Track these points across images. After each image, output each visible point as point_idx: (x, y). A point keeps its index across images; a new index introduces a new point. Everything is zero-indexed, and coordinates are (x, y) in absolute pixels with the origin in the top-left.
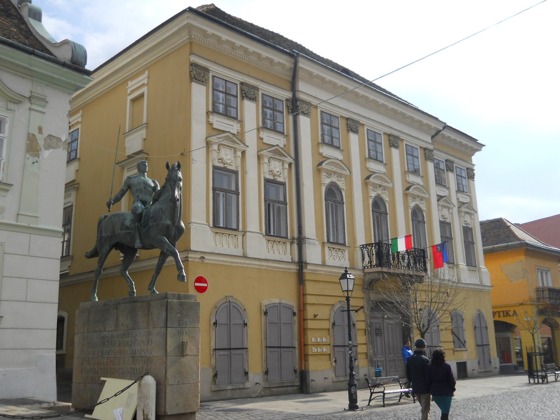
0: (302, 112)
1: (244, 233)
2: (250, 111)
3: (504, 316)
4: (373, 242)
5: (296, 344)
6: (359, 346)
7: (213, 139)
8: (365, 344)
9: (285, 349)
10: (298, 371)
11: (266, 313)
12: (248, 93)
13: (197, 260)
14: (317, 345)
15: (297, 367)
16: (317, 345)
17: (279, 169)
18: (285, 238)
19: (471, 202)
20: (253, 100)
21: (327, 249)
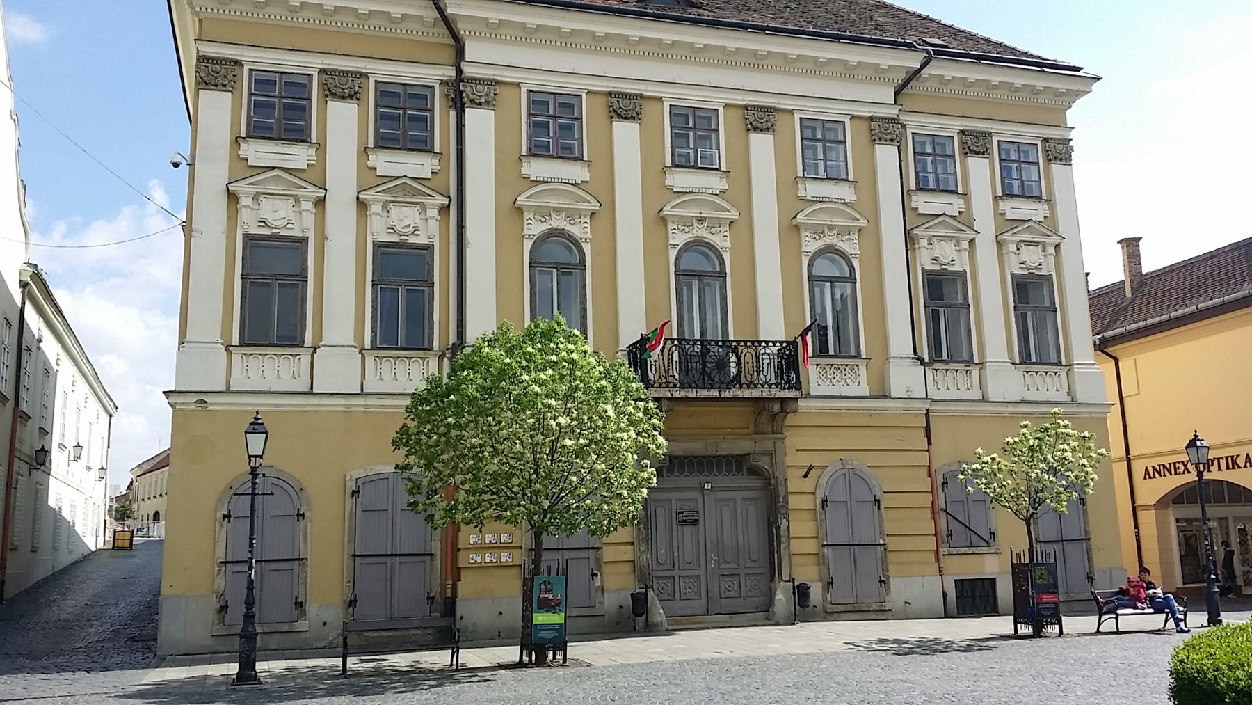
0: (472, 101)
1: (982, 364)
2: (343, 124)
3: (1228, 468)
4: (675, 336)
5: (437, 548)
6: (605, 548)
7: (1008, 236)
8: (633, 543)
9: (274, 566)
10: (438, 599)
11: (356, 493)
12: (975, 144)
13: (193, 407)
14: (481, 548)
15: (436, 592)
16: (481, 548)
17: (419, 224)
18: (854, 357)
19: (1051, 219)
20: (351, 97)
21: (370, 361)
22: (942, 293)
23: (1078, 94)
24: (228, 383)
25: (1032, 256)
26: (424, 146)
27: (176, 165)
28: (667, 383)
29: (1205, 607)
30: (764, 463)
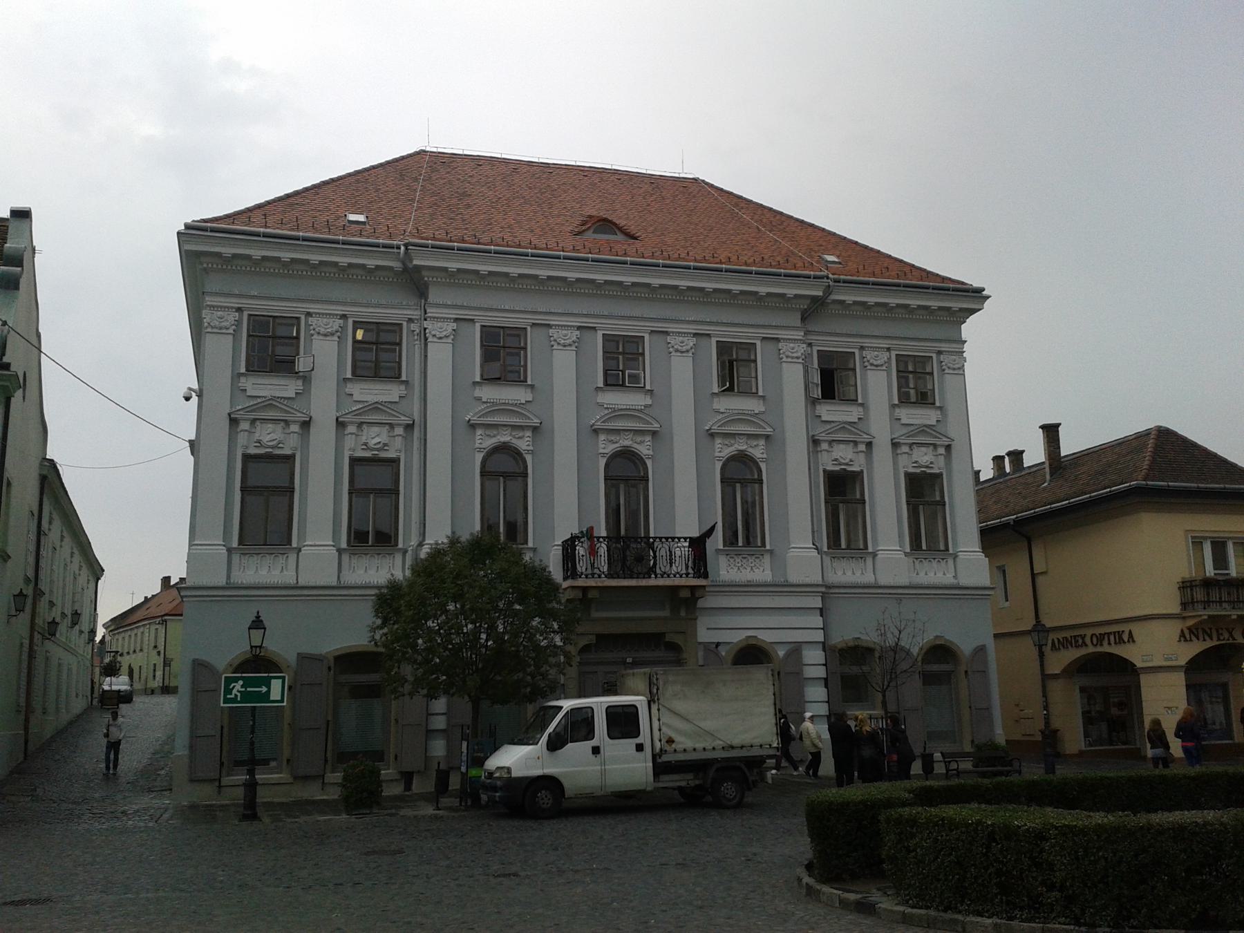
0: (677, 351)
21: (345, 557)
22: (842, 489)
23: (973, 311)
24: (229, 577)
25: (924, 457)
26: (395, 376)
27: (187, 399)
28: (593, 575)
29: (569, 792)
30: (678, 639)
